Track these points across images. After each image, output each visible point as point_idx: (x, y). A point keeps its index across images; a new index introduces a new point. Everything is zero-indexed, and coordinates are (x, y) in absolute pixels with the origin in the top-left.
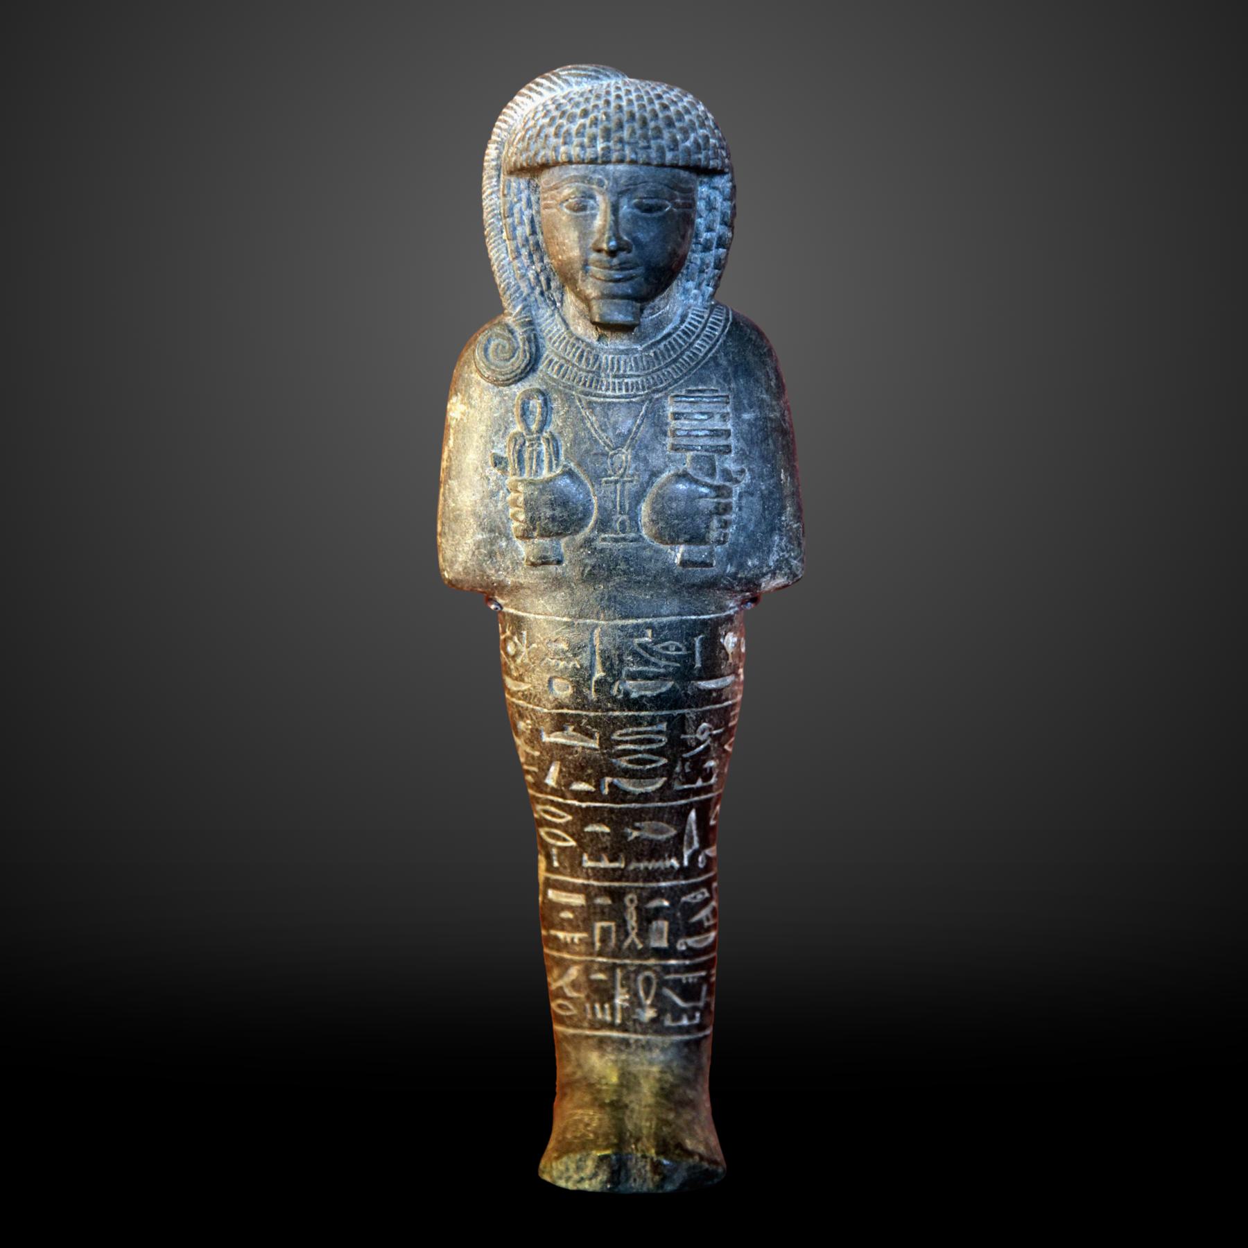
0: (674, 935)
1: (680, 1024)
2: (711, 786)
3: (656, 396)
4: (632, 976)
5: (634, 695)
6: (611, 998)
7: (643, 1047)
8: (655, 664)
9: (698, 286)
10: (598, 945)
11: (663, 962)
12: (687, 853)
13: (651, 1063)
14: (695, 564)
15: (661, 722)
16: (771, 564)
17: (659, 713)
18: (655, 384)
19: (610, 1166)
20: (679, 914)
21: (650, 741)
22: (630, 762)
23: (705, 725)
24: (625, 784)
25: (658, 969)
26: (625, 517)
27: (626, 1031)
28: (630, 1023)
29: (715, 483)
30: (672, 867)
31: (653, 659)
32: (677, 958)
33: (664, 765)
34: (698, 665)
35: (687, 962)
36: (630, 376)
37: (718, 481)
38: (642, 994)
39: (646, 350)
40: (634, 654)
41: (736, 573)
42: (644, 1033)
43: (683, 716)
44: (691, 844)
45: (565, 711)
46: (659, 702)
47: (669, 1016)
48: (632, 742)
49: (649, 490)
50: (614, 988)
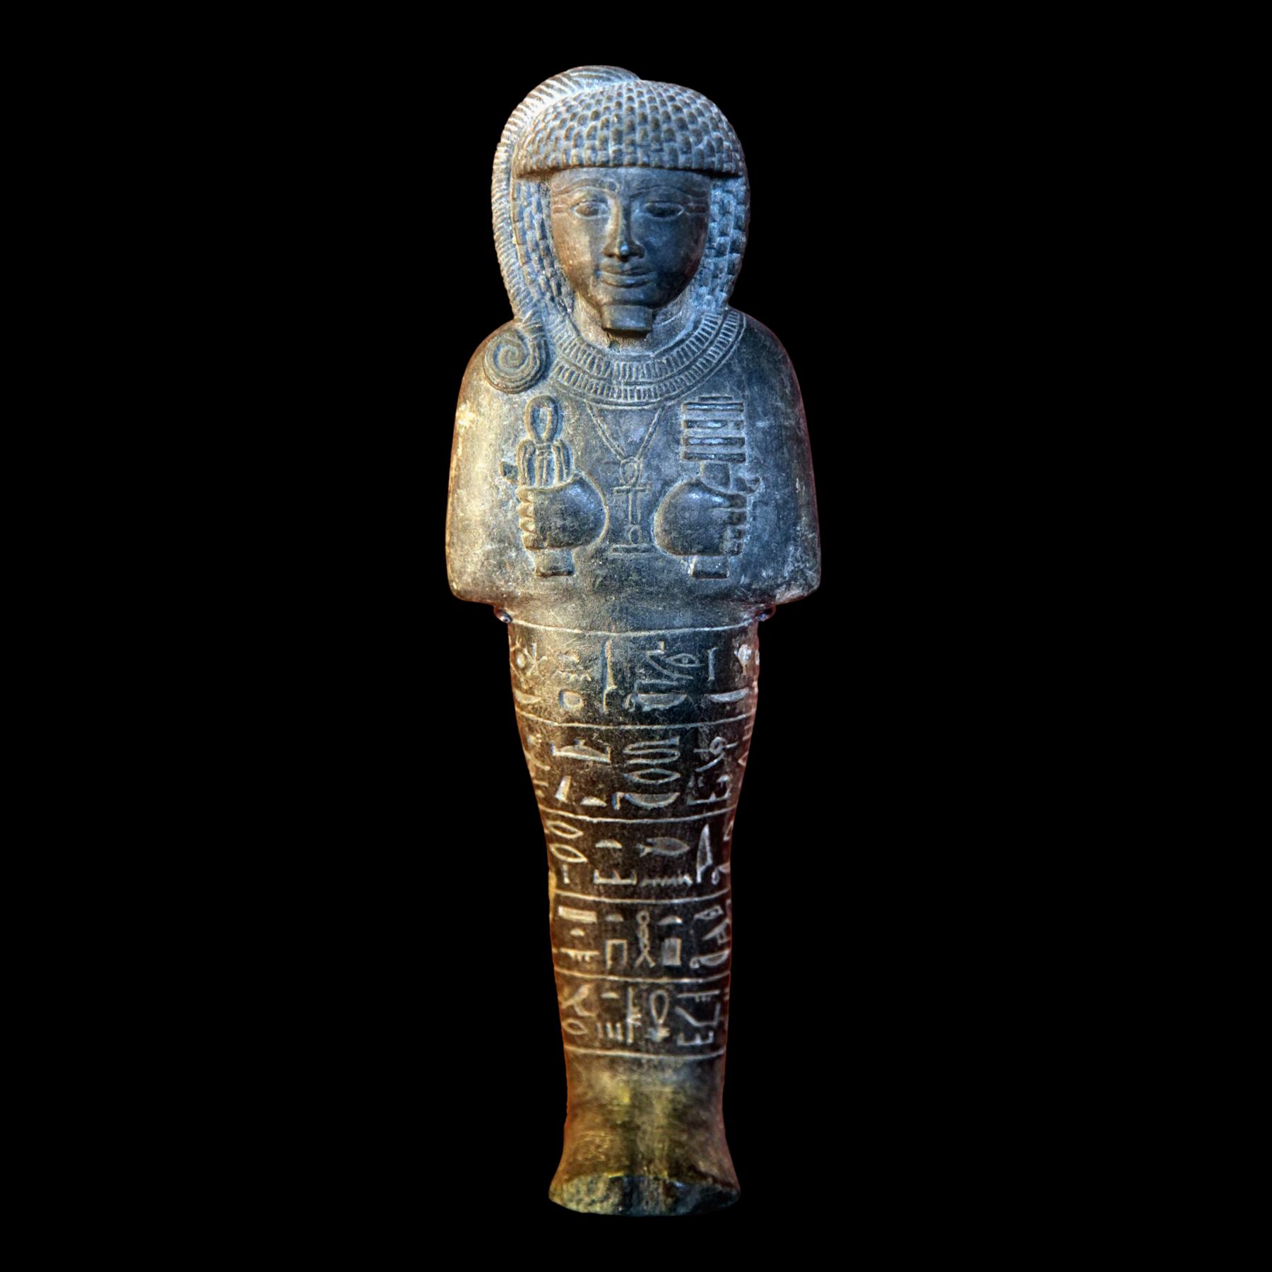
0: (687, 953)
1: (693, 1043)
2: (725, 801)
3: (669, 404)
4: (645, 994)
5: (646, 708)
6: (623, 1017)
7: (655, 1067)
8: (668, 677)
9: (712, 292)
10: (609, 963)
11: (676, 981)
12: (700, 870)
13: (663, 1083)
14: (708, 575)
15: (674, 735)
16: (786, 574)
17: (672, 727)
18: (668, 392)
19: (622, 1188)
20: (692, 932)
21: (663, 756)
22: (642, 776)
23: (718, 739)
24: (637, 799)
25: (671, 987)
26: (637, 527)
27: (638, 1050)
28: (642, 1043)
29: (729, 492)
30: (685, 884)
31: (665, 672)
32: (690, 976)
33: (677, 780)
34: (712, 678)
35: (701, 981)
36: (642, 384)
37: (732, 490)
38: (654, 1013)
39: (658, 356)
40: (647, 666)
41: (750, 584)
42: (657, 1053)
43: (696, 730)
44: (704, 860)
45: (576, 725)
46: (672, 715)
47: (682, 1035)
48: (644, 756)
49: (661, 499)
50: (626, 1007)
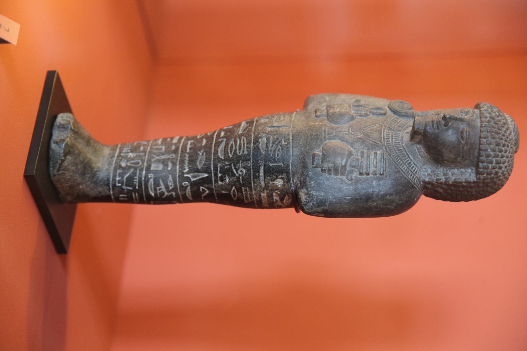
0: (156, 172)
1: (117, 176)
2: (217, 182)
3: (384, 148)
4: (140, 158)
5: (260, 140)
6: (132, 152)
7: (110, 162)
8: (272, 146)
9: (429, 174)
10: (155, 147)
11: (145, 169)
12: (189, 176)
13: (103, 164)
14: (314, 158)
15: (248, 151)
16: (312, 192)
17: (252, 150)
18: (389, 148)
19: (66, 124)
20: (164, 174)
21: (240, 149)
22: (232, 144)
23: (245, 171)
24: (222, 146)
25: (142, 167)
26: (334, 134)
27: (118, 157)
28: (120, 158)
29: (347, 166)
30: (185, 169)
31: (274, 145)
32: (145, 174)
33: (229, 156)
34: (271, 165)
35: (143, 179)
36: (392, 140)
37: (348, 168)
38: (132, 162)
39: (403, 146)
40: (277, 139)
41: (308, 177)
42: (116, 163)
43: (249, 160)
44: (194, 177)
45: (255, 122)
46: (257, 149)
47: (121, 171)
48: (240, 143)
49: (345, 143)
50: (136, 152)
